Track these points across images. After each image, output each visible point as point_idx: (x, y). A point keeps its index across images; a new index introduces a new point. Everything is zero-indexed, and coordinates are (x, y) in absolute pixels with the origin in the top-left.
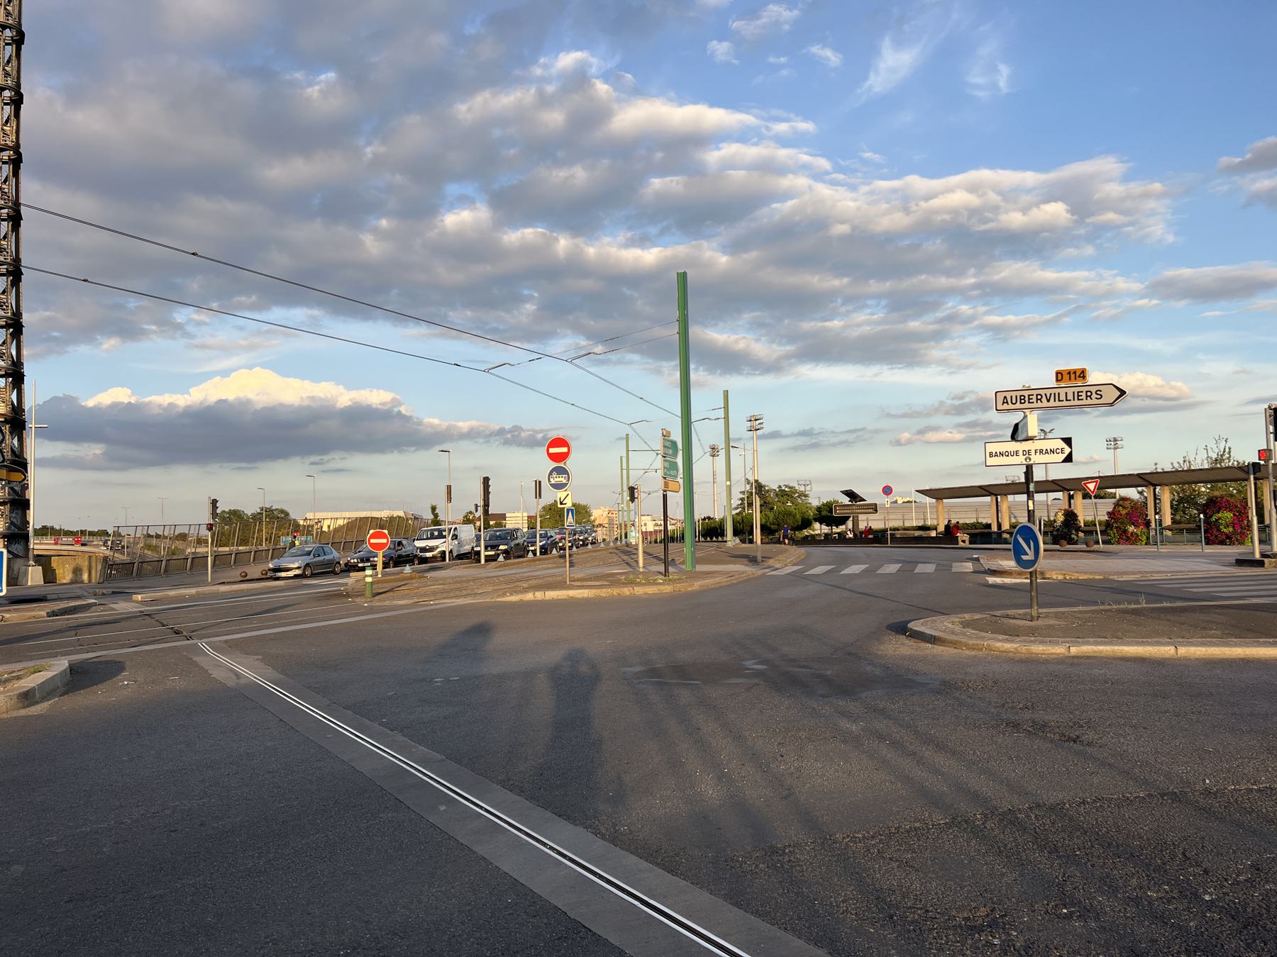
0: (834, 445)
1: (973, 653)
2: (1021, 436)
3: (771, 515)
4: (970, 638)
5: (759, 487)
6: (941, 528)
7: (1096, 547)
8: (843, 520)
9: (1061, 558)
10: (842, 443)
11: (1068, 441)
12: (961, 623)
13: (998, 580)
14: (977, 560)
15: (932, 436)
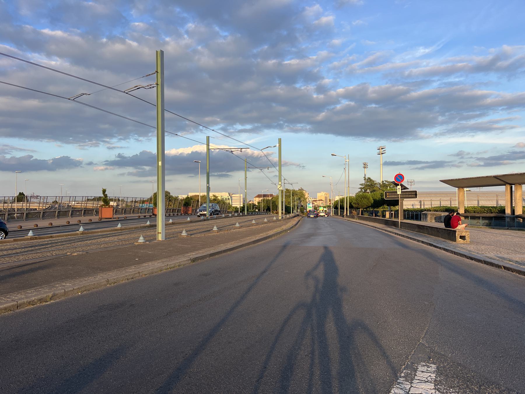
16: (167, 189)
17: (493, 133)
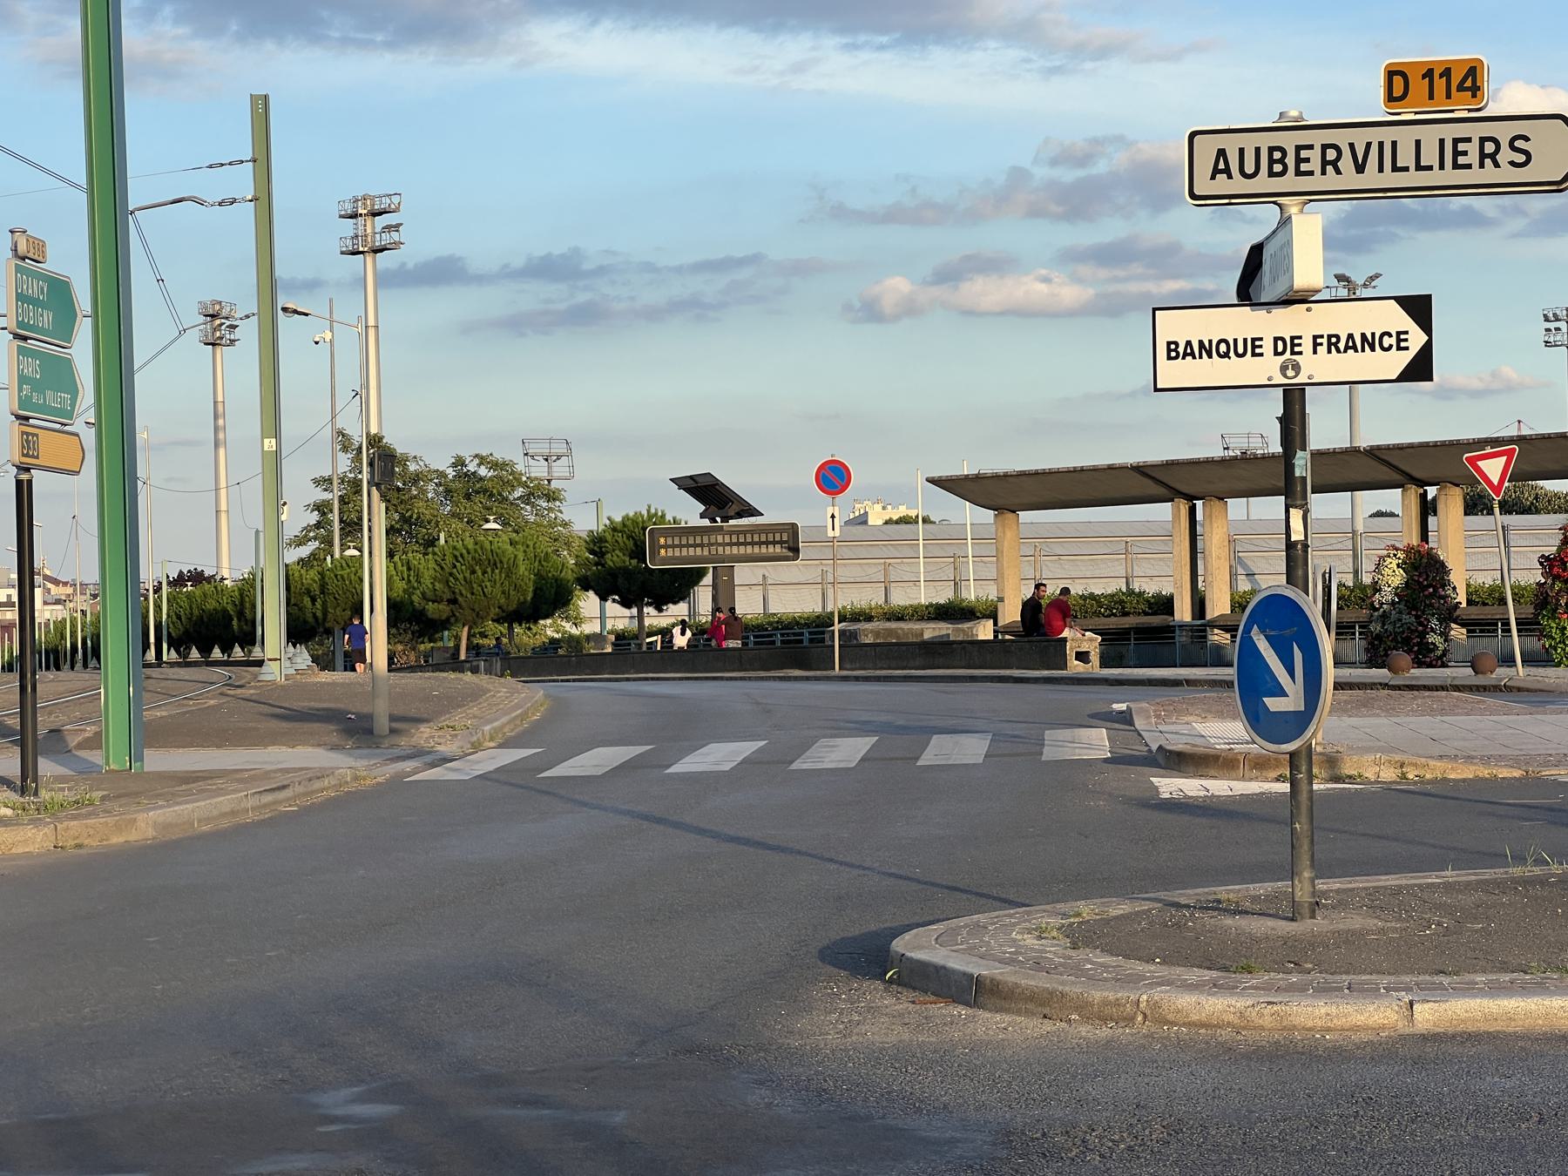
0: (654, 314)
1: (1104, 1032)
2: (1269, 288)
3: (427, 567)
4: (1093, 979)
5: (384, 460)
6: (1011, 613)
7: (1502, 674)
8: (676, 586)
9: (1390, 711)
10: (677, 307)
11: (1419, 308)
12: (1067, 931)
13: (1190, 786)
14: (1126, 718)
15: (984, 291)
16: (339, 426)
17: (518, 262)
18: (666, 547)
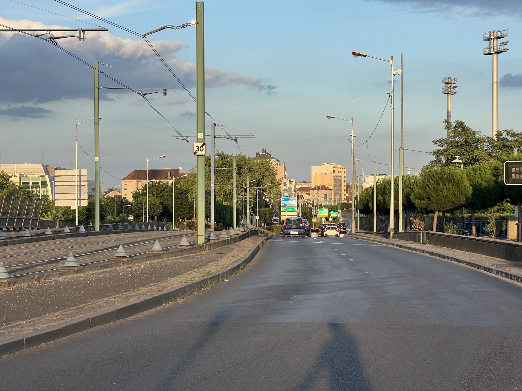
18: (515, 173)
